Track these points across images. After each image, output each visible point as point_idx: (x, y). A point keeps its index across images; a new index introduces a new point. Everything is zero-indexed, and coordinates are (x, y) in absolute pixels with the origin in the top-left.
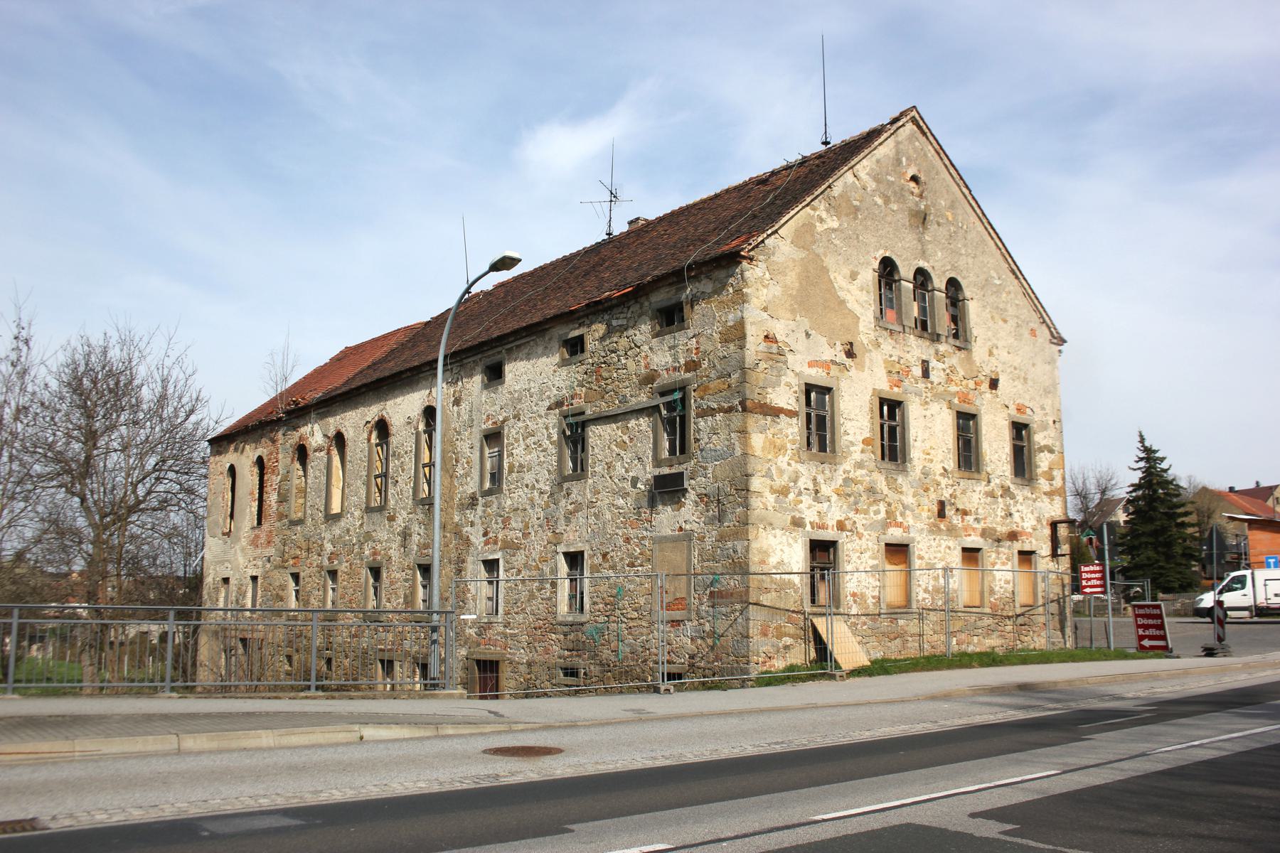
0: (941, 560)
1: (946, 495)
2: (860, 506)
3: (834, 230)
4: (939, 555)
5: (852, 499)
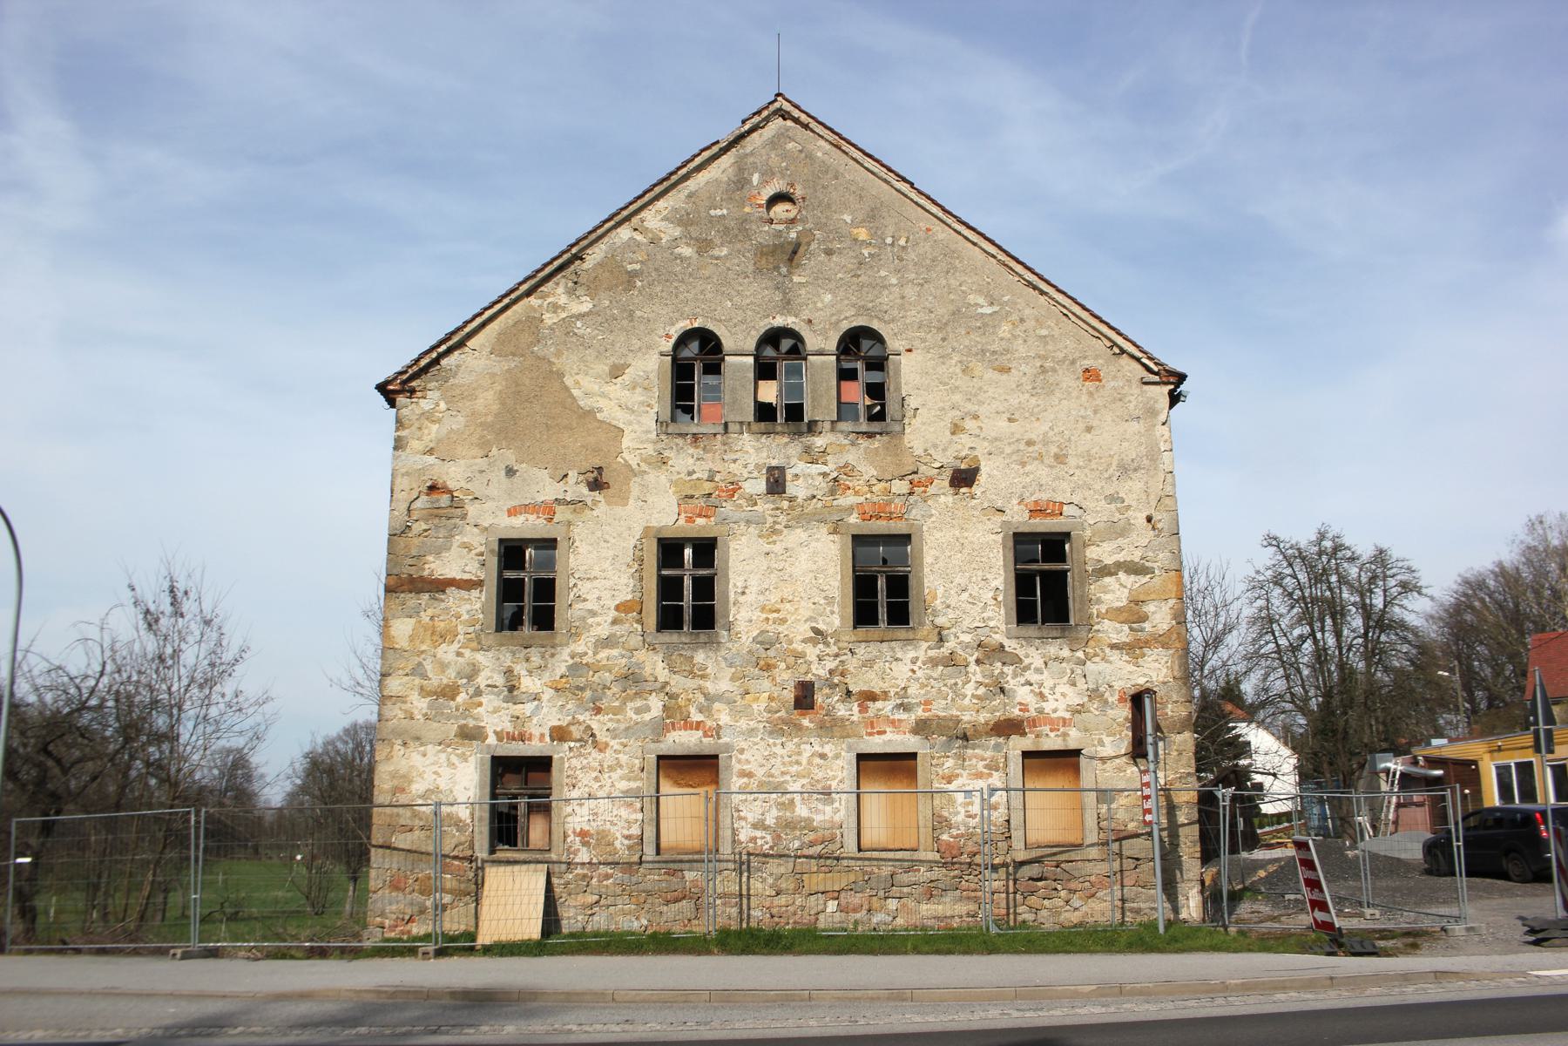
0: (798, 776)
1: (819, 671)
2: (604, 704)
3: (581, 316)
4: (795, 769)
5: (588, 694)
